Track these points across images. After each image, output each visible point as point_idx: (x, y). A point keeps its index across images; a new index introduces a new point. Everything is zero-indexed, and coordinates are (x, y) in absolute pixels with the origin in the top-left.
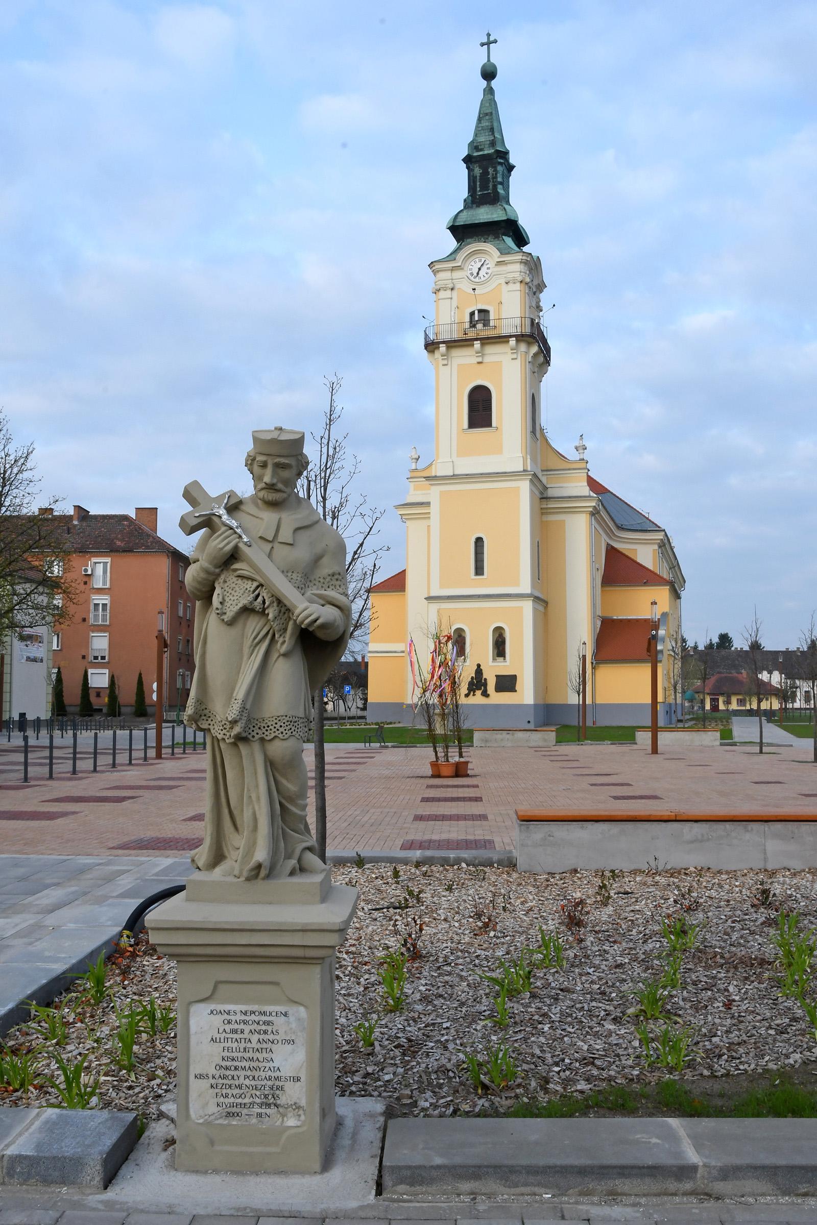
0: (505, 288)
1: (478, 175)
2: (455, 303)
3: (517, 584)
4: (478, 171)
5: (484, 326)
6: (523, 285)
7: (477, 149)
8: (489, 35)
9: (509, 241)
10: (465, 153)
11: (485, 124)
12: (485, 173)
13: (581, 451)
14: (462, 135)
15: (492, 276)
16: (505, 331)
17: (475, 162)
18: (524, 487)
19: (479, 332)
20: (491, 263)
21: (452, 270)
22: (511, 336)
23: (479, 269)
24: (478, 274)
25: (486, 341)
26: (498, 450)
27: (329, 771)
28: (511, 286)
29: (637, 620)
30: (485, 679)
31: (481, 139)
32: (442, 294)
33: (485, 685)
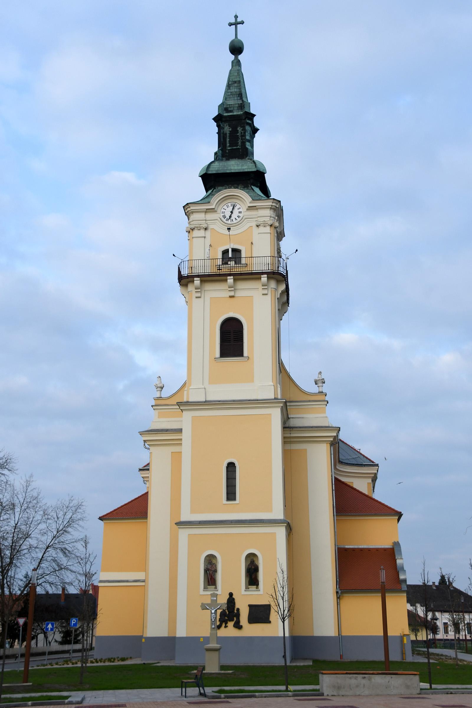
0: (256, 230)
1: (228, 132)
2: (208, 242)
4: (227, 129)
5: (236, 263)
6: (273, 228)
7: (227, 110)
8: (236, 17)
9: (257, 190)
10: (216, 113)
11: (234, 90)
13: (320, 385)
14: (214, 97)
15: (240, 219)
16: (256, 268)
17: (226, 121)
18: (276, 414)
19: (231, 267)
20: (243, 209)
21: (206, 212)
22: (263, 273)
23: (232, 212)
24: (230, 217)
25: (240, 277)
26: (249, 378)
28: (262, 229)
29: (369, 550)
30: (238, 610)
31: (231, 102)
32: (196, 233)
33: (238, 615)
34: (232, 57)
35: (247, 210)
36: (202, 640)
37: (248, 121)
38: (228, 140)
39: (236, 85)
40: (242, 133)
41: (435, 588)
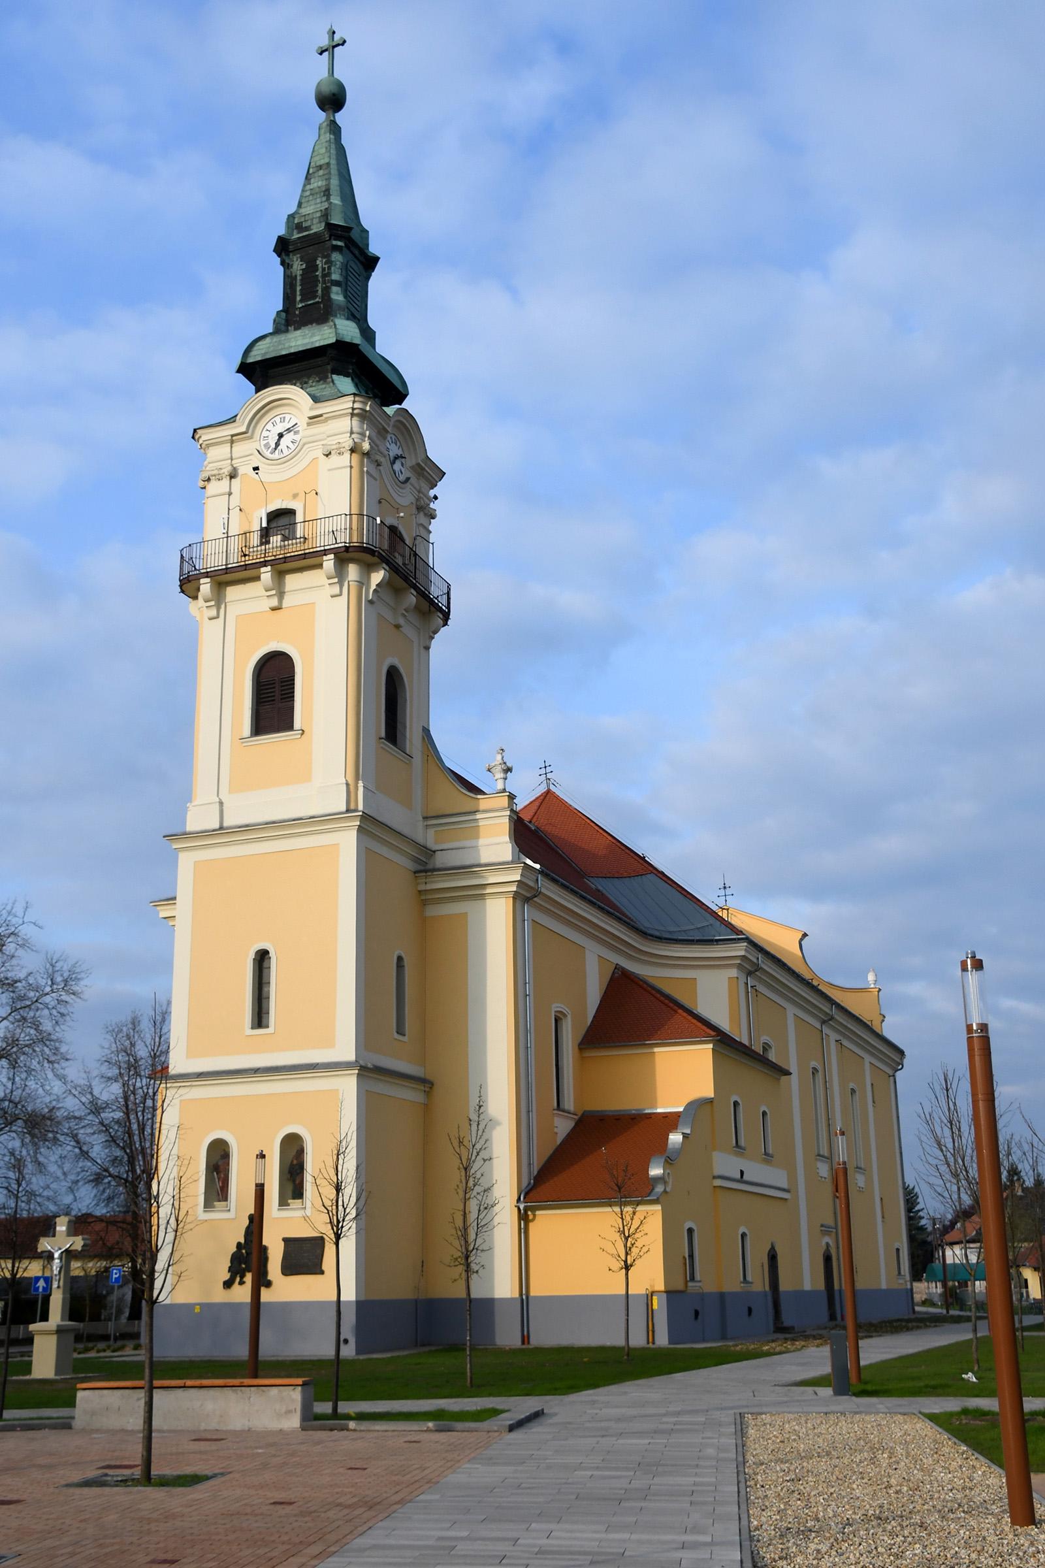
1: (299, 273)
3: (330, 1043)
4: (298, 266)
7: (300, 227)
12: (311, 267)
22: (325, 552)
24: (277, 444)
27: (651, 1331)
31: (307, 210)
34: (321, 116)
35: (309, 424)
36: (197, 1309)
37: (335, 243)
38: (298, 288)
39: (321, 173)
40: (324, 269)
41: (1020, 1193)
